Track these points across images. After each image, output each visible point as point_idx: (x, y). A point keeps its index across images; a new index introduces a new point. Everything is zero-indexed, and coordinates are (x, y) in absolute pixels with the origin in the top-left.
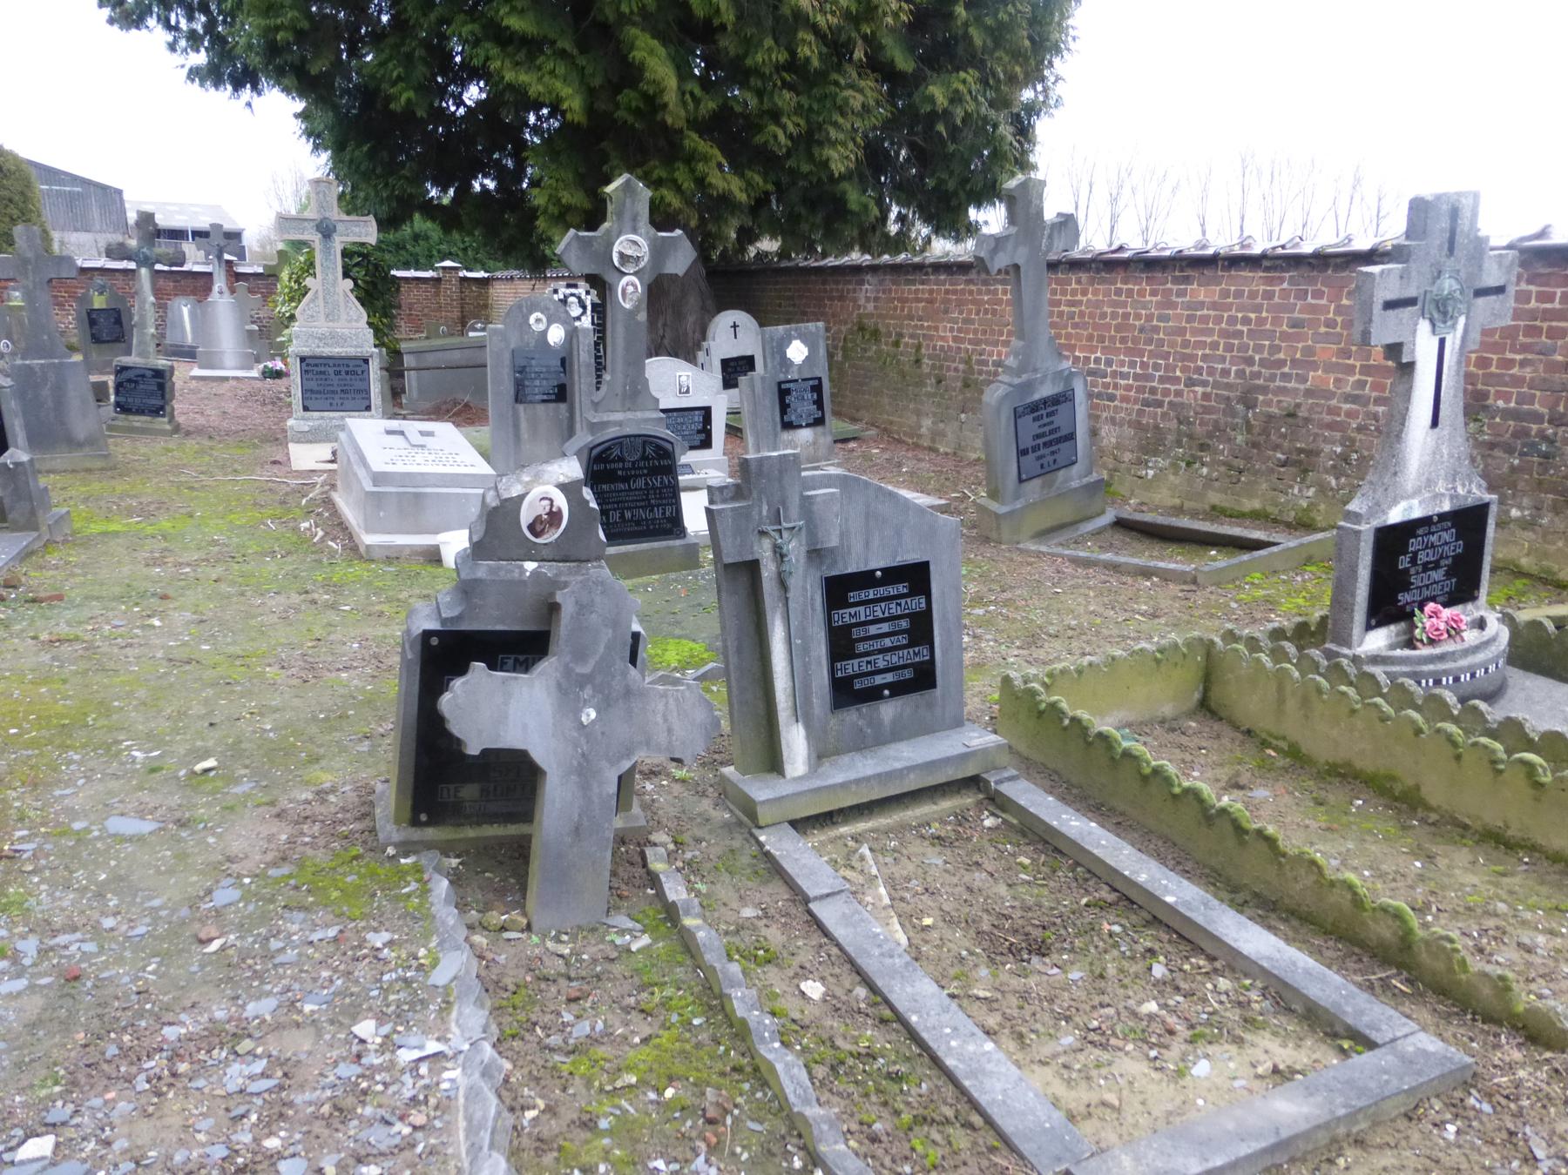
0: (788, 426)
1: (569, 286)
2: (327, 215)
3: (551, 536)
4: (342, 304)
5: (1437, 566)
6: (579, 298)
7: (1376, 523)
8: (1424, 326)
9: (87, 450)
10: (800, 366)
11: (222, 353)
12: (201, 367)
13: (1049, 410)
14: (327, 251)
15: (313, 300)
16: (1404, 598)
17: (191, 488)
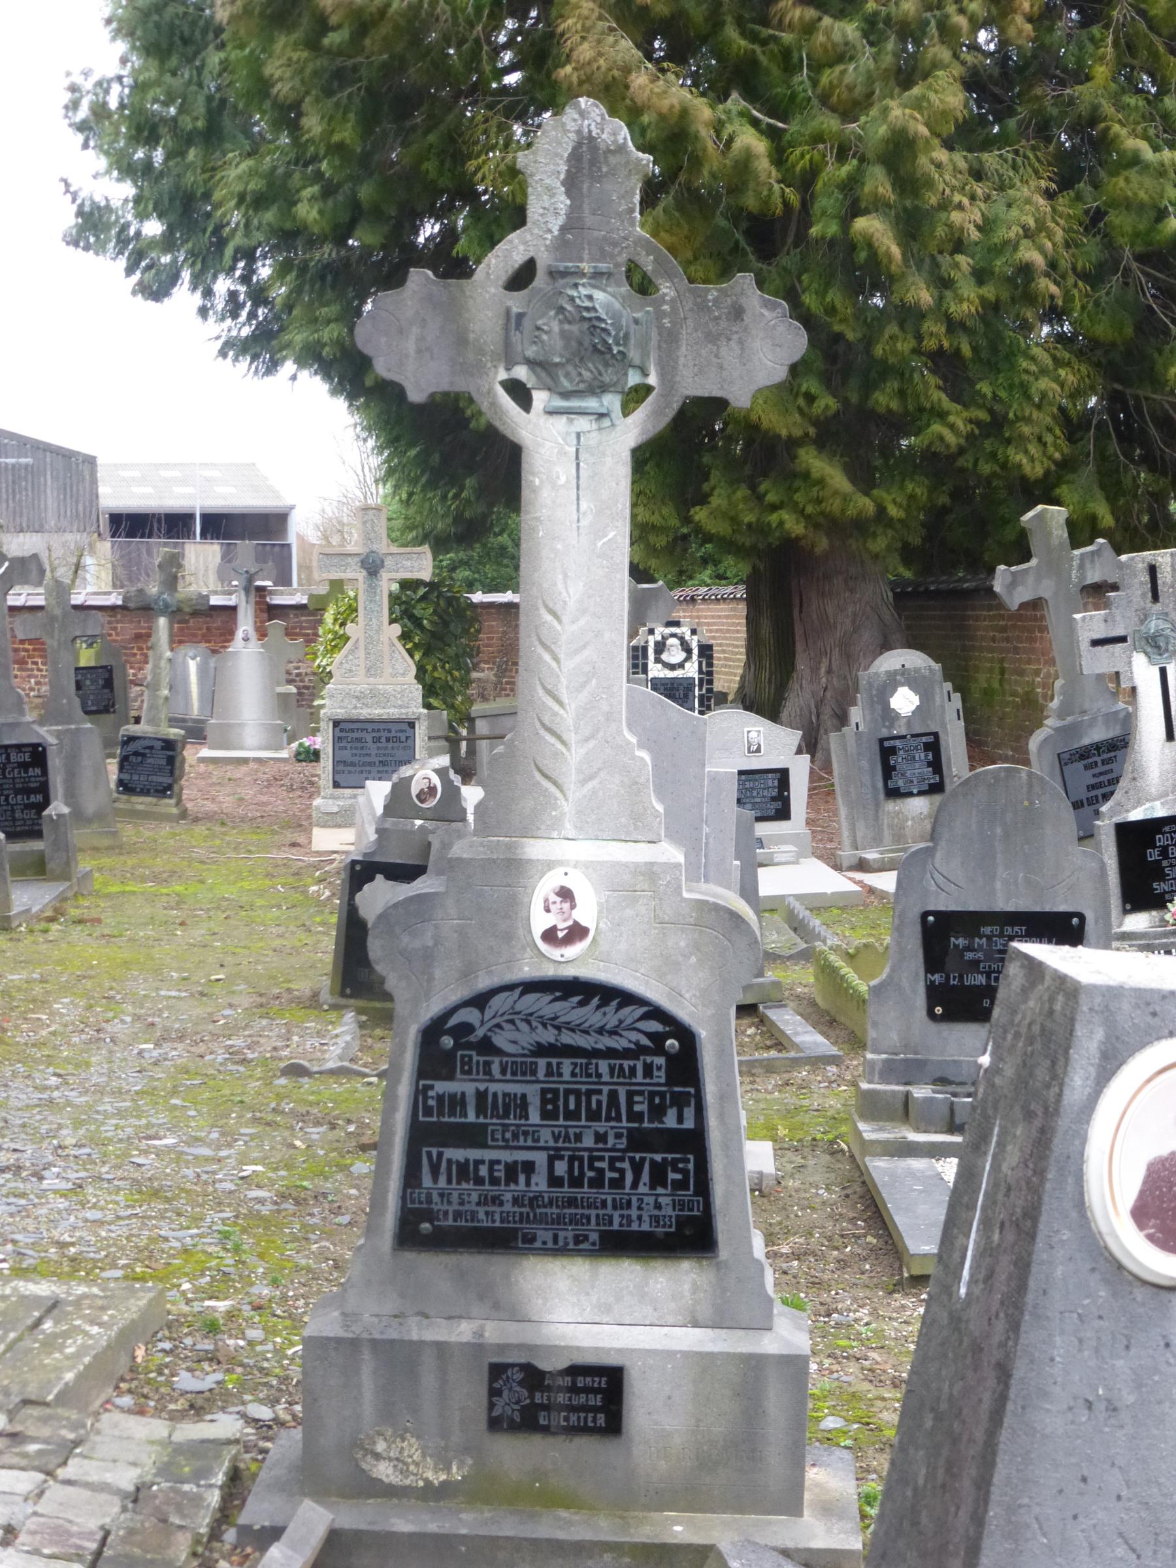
0: (894, 793)
2: (375, 547)
3: (431, 803)
4: (387, 657)
7: (1118, 819)
9: (95, 826)
10: (909, 720)
12: (211, 748)
13: (1106, 756)
14: (372, 589)
15: (352, 652)
16: (1159, 887)
17: (202, 862)
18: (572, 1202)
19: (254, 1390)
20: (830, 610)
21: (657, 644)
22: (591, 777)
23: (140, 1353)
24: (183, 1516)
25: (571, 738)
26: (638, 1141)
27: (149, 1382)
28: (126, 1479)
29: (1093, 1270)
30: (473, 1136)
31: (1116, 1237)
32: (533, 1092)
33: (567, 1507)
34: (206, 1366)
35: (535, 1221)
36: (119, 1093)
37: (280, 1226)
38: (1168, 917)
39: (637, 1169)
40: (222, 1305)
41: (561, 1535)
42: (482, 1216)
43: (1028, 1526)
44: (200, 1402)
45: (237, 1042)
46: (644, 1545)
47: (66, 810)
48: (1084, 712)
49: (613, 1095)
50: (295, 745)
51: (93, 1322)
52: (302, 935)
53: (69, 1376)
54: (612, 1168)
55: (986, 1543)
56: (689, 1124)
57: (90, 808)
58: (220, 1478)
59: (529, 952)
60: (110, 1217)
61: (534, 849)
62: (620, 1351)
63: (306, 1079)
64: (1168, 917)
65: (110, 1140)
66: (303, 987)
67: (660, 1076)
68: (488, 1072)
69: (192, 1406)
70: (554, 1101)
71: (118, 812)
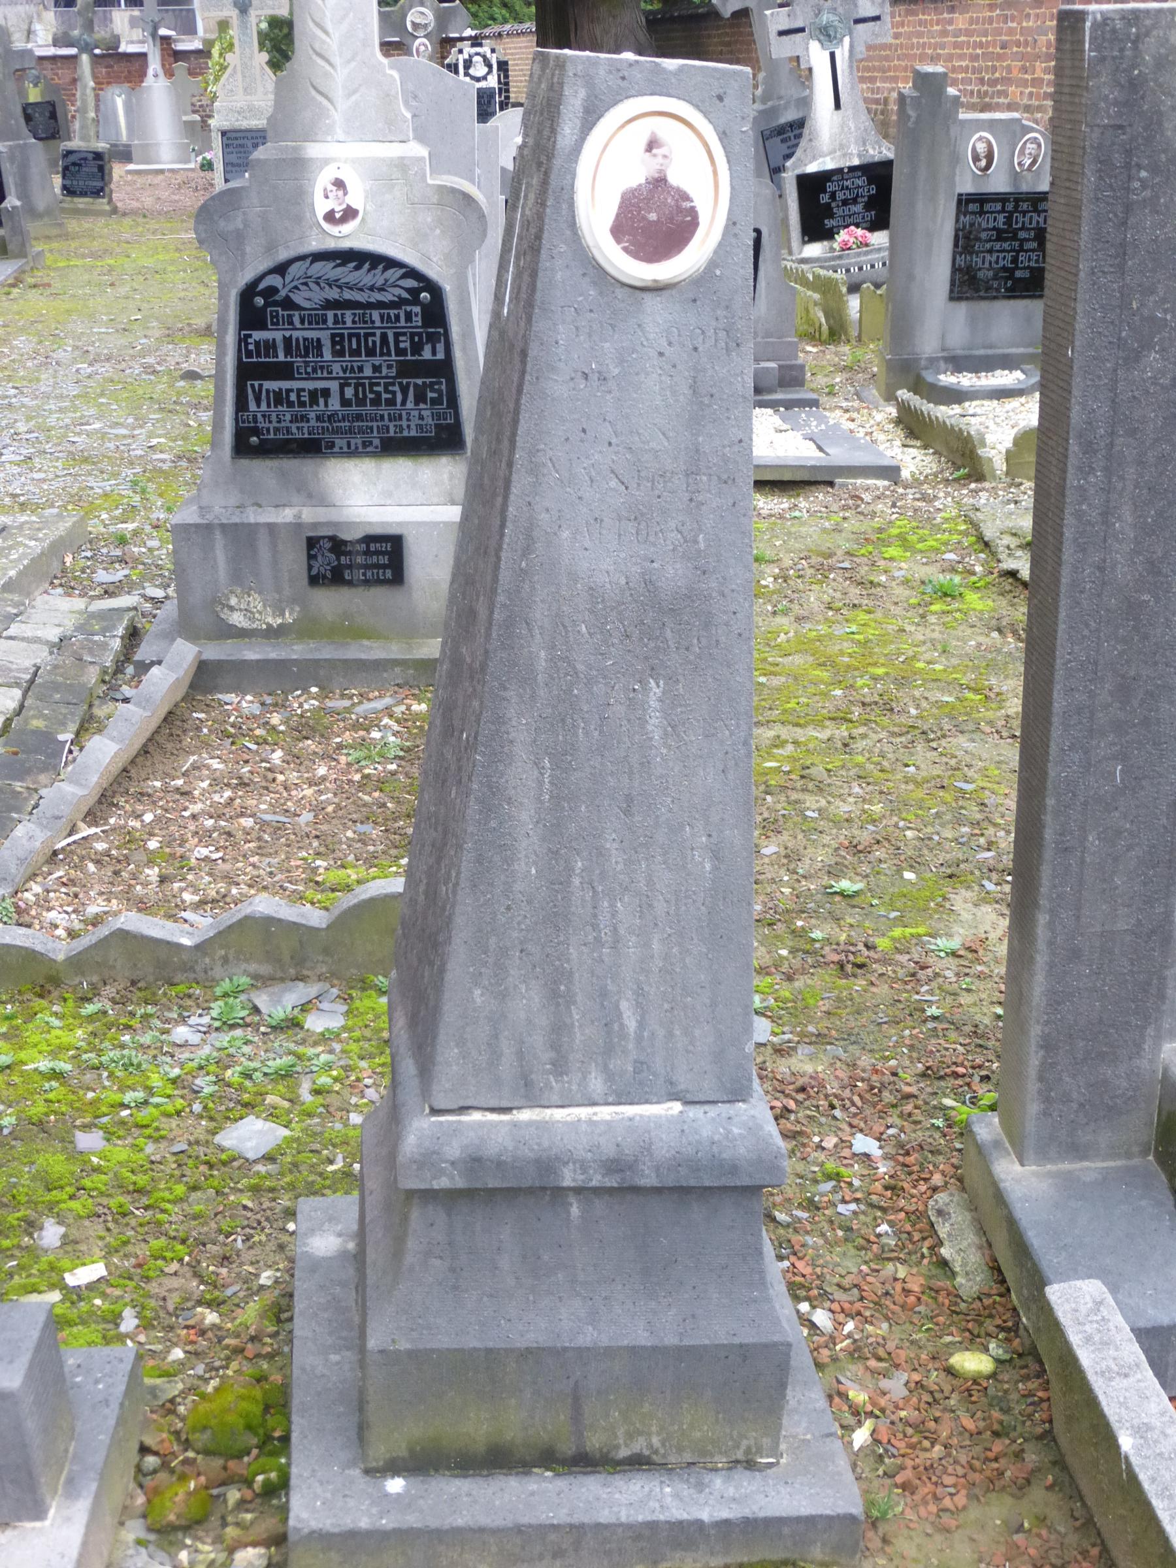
1: (473, 45)
5: (855, 201)
6: (484, 57)
7: (799, 171)
8: (814, 46)
9: (46, 219)
11: (158, 145)
14: (244, 25)
15: (231, 75)
16: (829, 223)
18: (359, 417)
19: (152, 580)
20: (598, 33)
21: (465, 61)
22: (355, 92)
23: (68, 560)
24: (94, 656)
25: (337, 60)
26: (406, 370)
27: (75, 578)
28: (53, 634)
29: (584, 275)
30: (284, 371)
31: (609, 261)
32: (325, 336)
33: (369, 638)
34: (117, 566)
35: (333, 432)
36: (61, 397)
37: (176, 476)
38: (836, 245)
39: (405, 390)
40: (131, 526)
41: (363, 656)
42: (294, 430)
43: (544, 465)
44: (111, 588)
45: (150, 360)
46: (423, 660)
47: (18, 203)
48: (780, 98)
49: (384, 337)
50: (200, 159)
51: (31, 539)
52: (202, 289)
53: (12, 573)
54: (387, 391)
55: (515, 477)
56: (440, 356)
57: (41, 204)
58: (120, 631)
59: (315, 231)
60: (51, 476)
61: (313, 150)
62: (399, 524)
63: (199, 382)
64: (836, 245)
65: (53, 427)
66: (200, 322)
67: (418, 321)
68: (291, 323)
69: (106, 592)
70: (341, 342)
71: (63, 210)
